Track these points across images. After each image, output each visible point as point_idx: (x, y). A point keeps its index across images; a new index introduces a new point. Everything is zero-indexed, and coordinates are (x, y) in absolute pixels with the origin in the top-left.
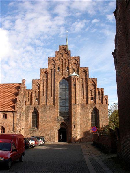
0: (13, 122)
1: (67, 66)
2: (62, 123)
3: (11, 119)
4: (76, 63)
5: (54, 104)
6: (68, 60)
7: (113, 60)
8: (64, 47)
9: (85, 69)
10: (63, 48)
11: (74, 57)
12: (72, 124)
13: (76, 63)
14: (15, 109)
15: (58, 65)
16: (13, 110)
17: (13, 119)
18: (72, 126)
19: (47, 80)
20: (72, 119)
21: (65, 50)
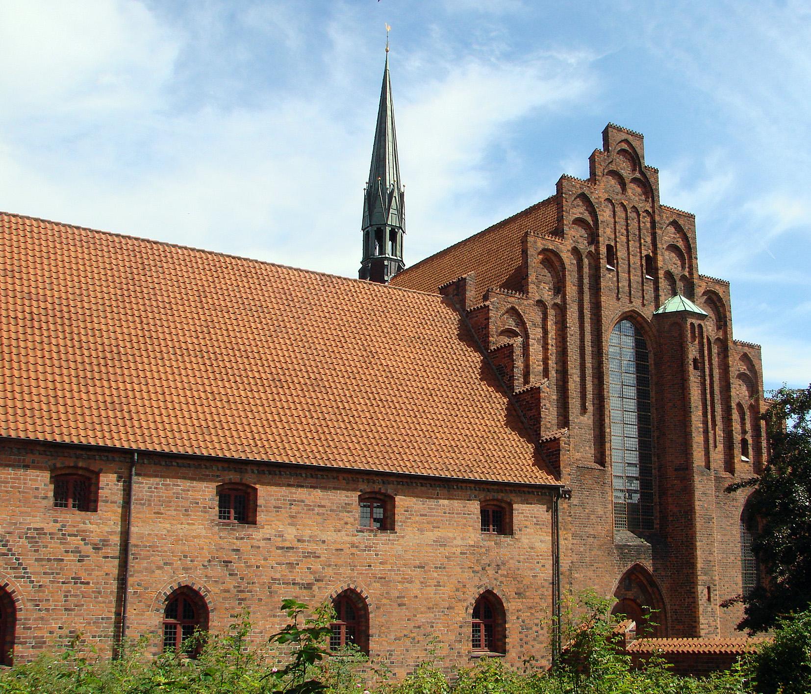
0: (549, 563)
1: (644, 253)
2: (637, 569)
3: (542, 542)
4: (681, 244)
5: (601, 459)
6: (649, 219)
7: (360, 256)
8: (630, 138)
9: (717, 287)
10: (625, 146)
11: (672, 211)
12: (701, 578)
13: (681, 244)
14: (558, 476)
15: (609, 231)
16: (542, 478)
17: (134, 529)
18: (700, 588)
19: (561, 310)
20: (699, 553)
21: (634, 157)
